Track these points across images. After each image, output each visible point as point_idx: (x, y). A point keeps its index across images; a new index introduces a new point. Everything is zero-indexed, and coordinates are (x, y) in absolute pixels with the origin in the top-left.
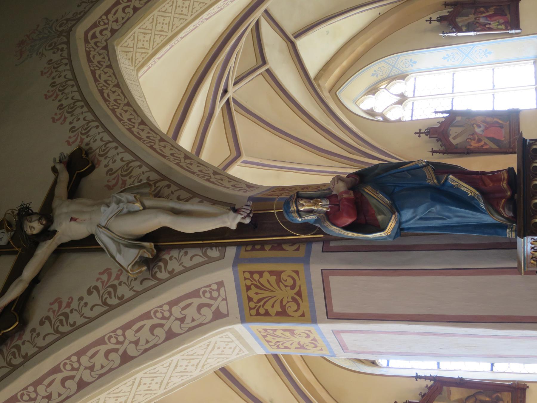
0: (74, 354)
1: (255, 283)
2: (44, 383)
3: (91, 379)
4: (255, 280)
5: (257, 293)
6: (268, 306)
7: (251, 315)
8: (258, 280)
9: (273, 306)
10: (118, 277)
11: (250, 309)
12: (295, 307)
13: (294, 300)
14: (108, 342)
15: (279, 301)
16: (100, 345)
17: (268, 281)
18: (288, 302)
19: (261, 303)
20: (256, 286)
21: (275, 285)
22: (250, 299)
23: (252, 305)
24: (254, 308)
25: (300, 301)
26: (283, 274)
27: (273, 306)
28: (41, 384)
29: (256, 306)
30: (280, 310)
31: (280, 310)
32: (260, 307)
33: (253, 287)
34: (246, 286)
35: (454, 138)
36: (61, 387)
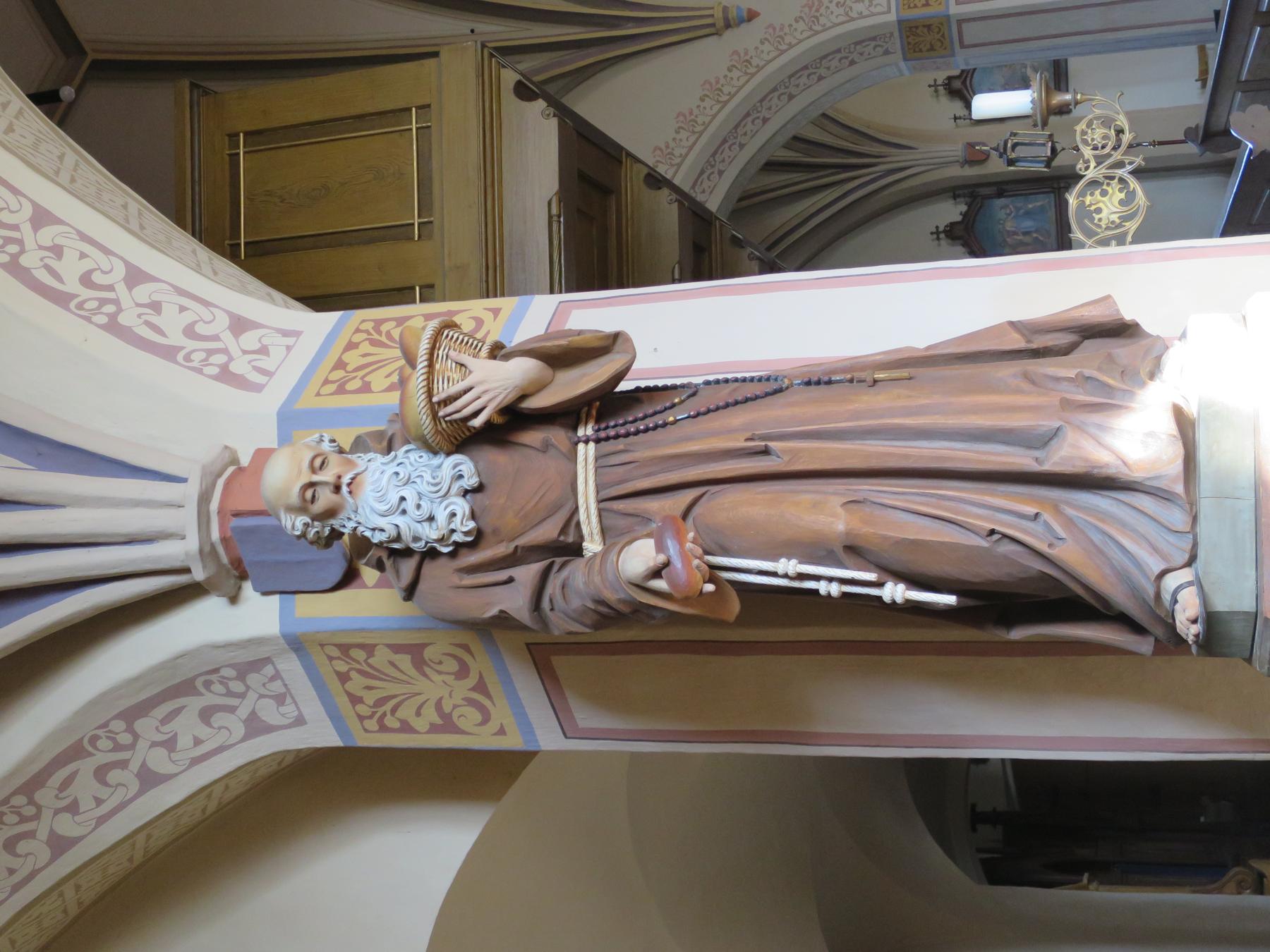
0: (118, 716)
1: (358, 666)
2: (49, 783)
3: (171, 769)
4: (358, 662)
5: (369, 688)
6: (406, 712)
7: (366, 731)
8: (365, 661)
9: (418, 714)
10: (817, 11)
11: (361, 718)
12: (478, 717)
13: (471, 702)
14: (90, 749)
15: (432, 703)
16: (186, 694)
17: (392, 664)
18: (455, 707)
19: (388, 707)
20: (360, 672)
21: (413, 672)
22: (355, 700)
23: (363, 709)
24: (371, 717)
25: (487, 703)
26: (242, 731)
27: (418, 714)
28: (258, 671)
29: (374, 713)
30: (438, 721)
31: (438, 721)
32: (384, 714)
33: (353, 674)
34: (338, 674)
35: (1042, 209)
36: (98, 785)
